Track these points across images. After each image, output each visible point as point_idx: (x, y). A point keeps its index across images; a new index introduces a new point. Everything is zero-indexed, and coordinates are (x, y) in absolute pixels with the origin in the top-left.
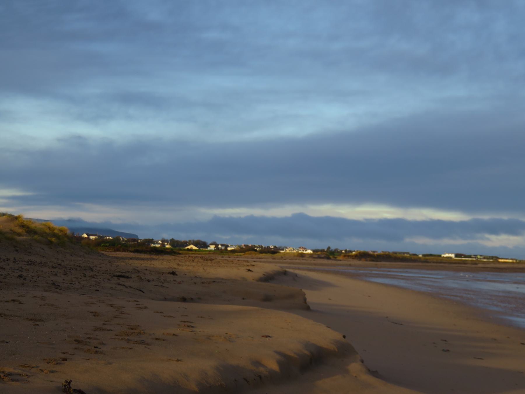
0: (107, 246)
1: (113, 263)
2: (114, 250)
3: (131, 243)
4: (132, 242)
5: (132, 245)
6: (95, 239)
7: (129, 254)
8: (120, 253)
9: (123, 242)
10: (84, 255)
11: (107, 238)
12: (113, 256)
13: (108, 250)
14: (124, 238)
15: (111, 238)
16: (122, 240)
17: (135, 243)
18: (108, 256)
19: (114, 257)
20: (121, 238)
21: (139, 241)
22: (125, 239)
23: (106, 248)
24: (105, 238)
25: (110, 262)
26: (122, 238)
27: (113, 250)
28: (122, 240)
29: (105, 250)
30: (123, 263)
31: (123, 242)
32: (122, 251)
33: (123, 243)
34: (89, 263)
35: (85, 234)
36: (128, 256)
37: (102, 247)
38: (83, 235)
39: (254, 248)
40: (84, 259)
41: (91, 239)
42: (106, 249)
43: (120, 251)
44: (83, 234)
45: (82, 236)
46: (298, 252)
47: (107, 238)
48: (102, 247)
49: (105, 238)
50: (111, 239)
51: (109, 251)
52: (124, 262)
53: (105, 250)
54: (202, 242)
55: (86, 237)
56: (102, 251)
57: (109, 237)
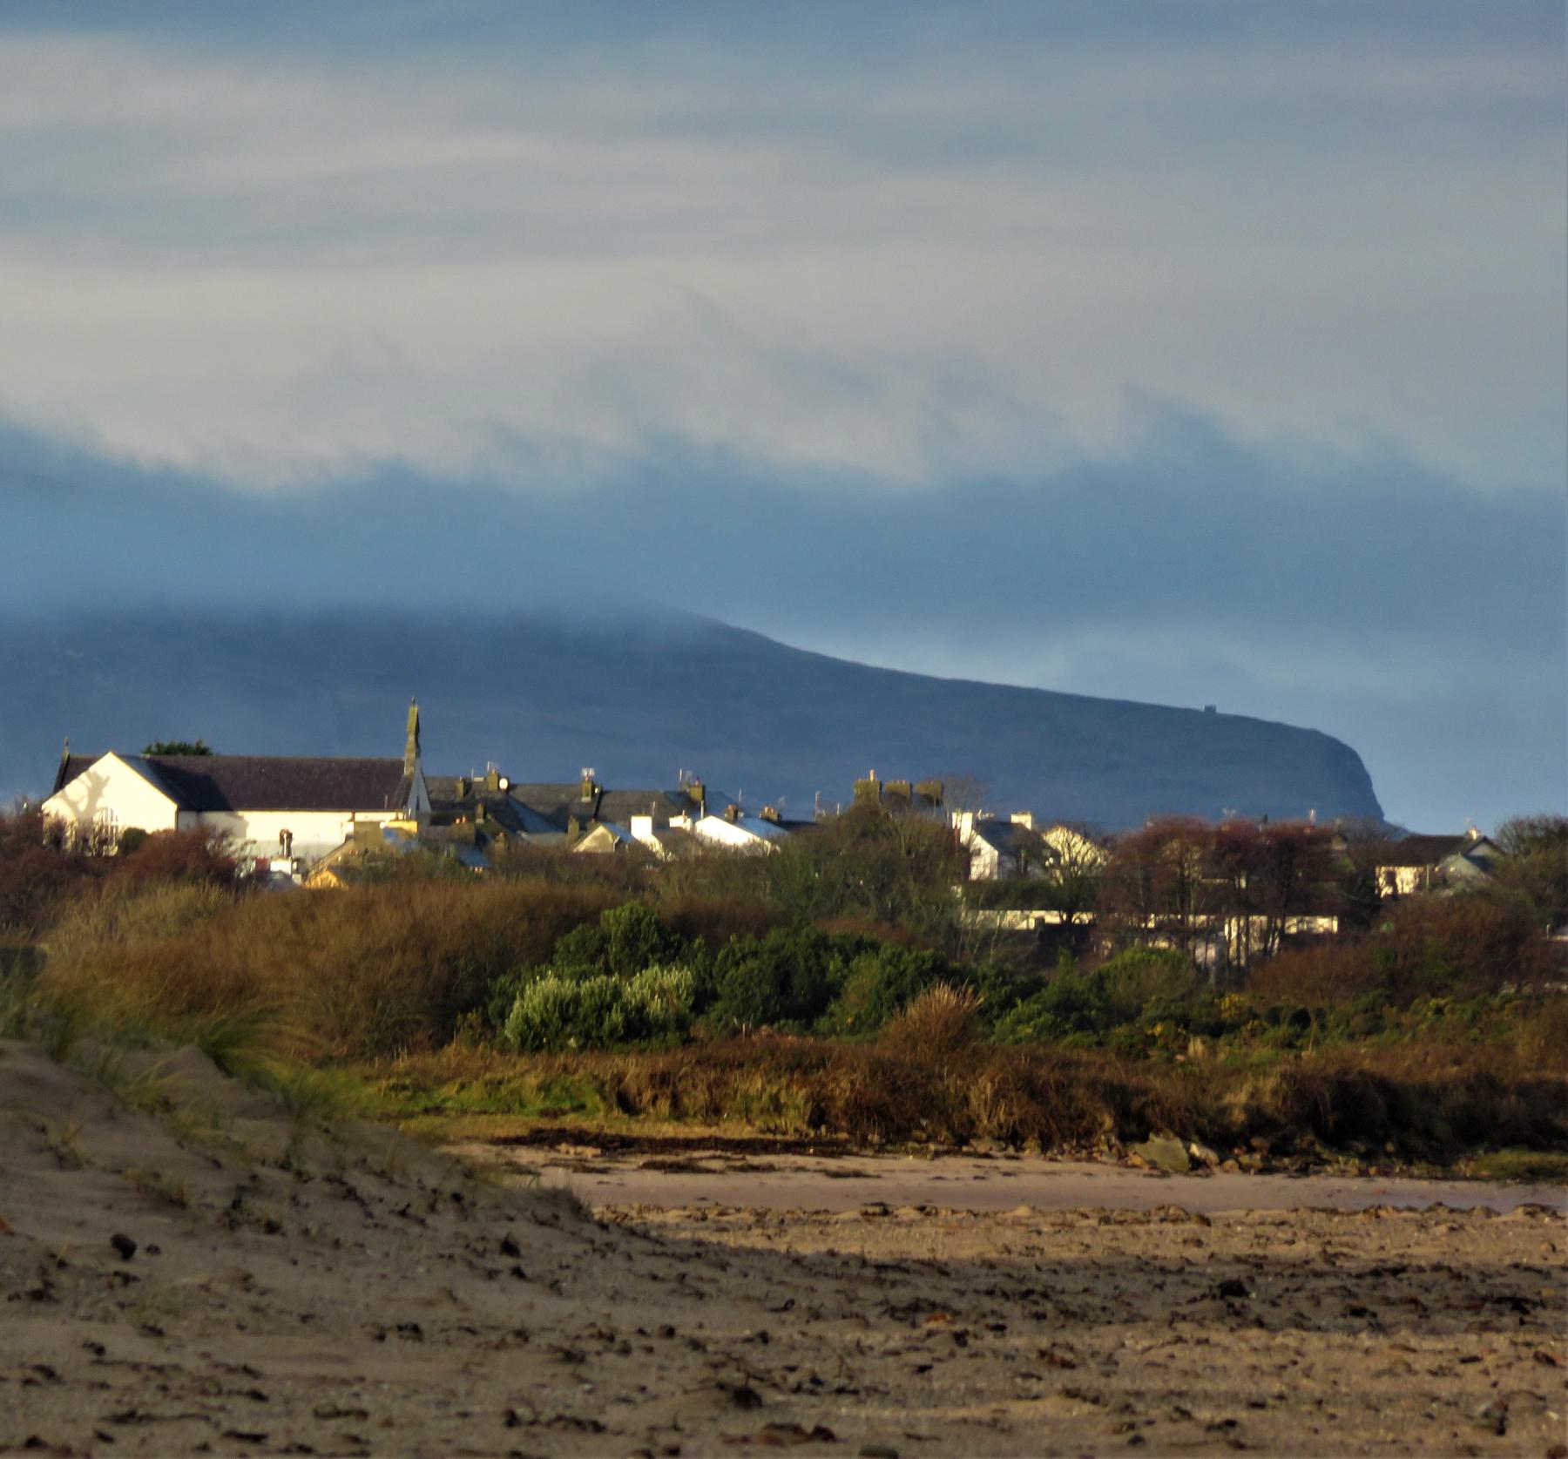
0: (638, 1028)
1: (807, 1414)
2: (818, 1117)
3: (1210, 934)
4: (1245, 906)
5: (1231, 974)
6: (344, 870)
7: (1185, 1188)
8: (958, 1168)
9: (1024, 920)
10: (124, 1248)
11: (642, 828)
12: (809, 1248)
13: (678, 1113)
14: (1045, 823)
15: (718, 831)
16: (985, 860)
17: (1306, 940)
18: (699, 1250)
19: (833, 1266)
20: (964, 823)
21: (1406, 878)
22: (1056, 838)
23: (633, 1068)
24: (597, 839)
25: (745, 1398)
26: (993, 830)
27: (793, 1122)
28: (985, 860)
29: (604, 1120)
30: (1051, 1407)
31: (1024, 920)
32: (1013, 1138)
33: (1014, 935)
34: (244, 1417)
35: (110, 766)
36: (1168, 1244)
37: (536, 1039)
38: (77, 788)
39: (643, 863)
40: (122, 1341)
41: (262, 872)
42: (627, 1105)
43: (960, 1141)
44: (68, 771)
45: (56, 807)
46: (213, 837)
47: (642, 828)
48: (536, 1039)
49: (597, 839)
50: (723, 861)
51: (697, 1131)
52: (1082, 1378)
53: (604, 1120)
54: (525, 1147)
55: (134, 839)
56: (536, 1139)
57: (692, 809)
